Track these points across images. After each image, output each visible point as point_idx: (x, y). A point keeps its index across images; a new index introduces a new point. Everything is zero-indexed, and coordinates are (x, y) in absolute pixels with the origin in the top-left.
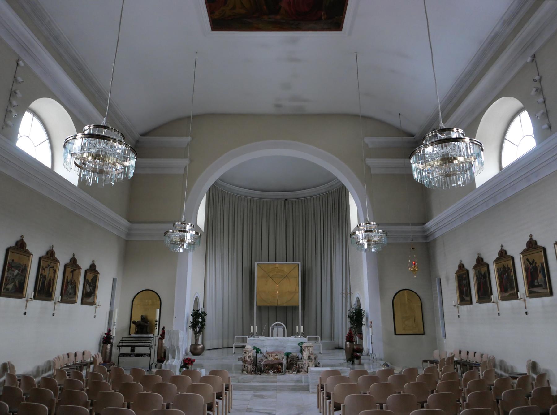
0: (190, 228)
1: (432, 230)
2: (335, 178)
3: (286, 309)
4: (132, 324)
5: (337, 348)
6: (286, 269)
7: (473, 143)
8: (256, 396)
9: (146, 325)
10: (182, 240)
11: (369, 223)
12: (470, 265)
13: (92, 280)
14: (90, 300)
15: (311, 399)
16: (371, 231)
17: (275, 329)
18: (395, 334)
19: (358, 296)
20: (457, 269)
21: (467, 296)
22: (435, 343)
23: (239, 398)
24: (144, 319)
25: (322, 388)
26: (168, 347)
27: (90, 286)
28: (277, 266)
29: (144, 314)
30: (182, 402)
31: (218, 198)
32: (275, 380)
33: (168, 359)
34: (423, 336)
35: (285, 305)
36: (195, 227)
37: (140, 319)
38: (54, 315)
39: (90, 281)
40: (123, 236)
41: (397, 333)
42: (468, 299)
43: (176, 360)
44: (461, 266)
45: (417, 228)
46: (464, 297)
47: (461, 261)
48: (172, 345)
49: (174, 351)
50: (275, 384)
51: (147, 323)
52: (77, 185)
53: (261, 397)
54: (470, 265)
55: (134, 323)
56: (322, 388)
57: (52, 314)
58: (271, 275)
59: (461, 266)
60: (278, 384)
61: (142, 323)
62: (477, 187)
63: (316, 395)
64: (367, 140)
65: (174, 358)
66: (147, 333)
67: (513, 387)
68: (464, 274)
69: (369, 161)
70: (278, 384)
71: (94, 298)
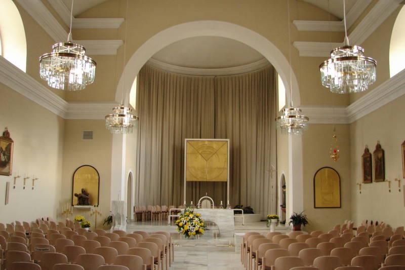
0: (128, 111)
1: (354, 112)
2: (263, 58)
3: (214, 184)
4: (74, 196)
5: (262, 221)
6: (215, 146)
7: (367, 61)
8: (190, 255)
9: (87, 197)
10: (121, 124)
11: (293, 109)
12: (372, 150)
13: (6, 148)
14: (5, 170)
15: (235, 258)
16: (294, 117)
17: (204, 201)
18: (315, 207)
19: (283, 173)
20: (363, 152)
21: (369, 176)
22: (350, 215)
23: (179, 255)
24: (84, 191)
25: (245, 246)
26: (115, 215)
27: (4, 155)
28: (206, 143)
29: (84, 188)
30: (125, 261)
31: (147, 76)
32: (206, 243)
33: (115, 225)
34: (340, 209)
35: (214, 180)
36: (130, 108)
37: (81, 192)
38: (24, 188)
39: (4, 150)
40: (63, 116)
41: (316, 206)
42: (369, 178)
43: (121, 226)
44: (367, 151)
45: (340, 110)
46: (367, 178)
47: (378, 141)
48: (118, 213)
49: (120, 218)
50: (206, 246)
51: (88, 196)
52: (25, 71)
53: (195, 255)
54: (372, 150)
55: (76, 195)
56: (245, 246)
57: (23, 188)
58: (200, 152)
59: (367, 151)
60: (208, 246)
61: (83, 195)
62: (391, 77)
63: (240, 255)
64: (296, 23)
65: (119, 224)
66: (88, 205)
67: (355, 236)
68: (368, 157)
69: (297, 44)
70: (208, 246)
71: (9, 168)
